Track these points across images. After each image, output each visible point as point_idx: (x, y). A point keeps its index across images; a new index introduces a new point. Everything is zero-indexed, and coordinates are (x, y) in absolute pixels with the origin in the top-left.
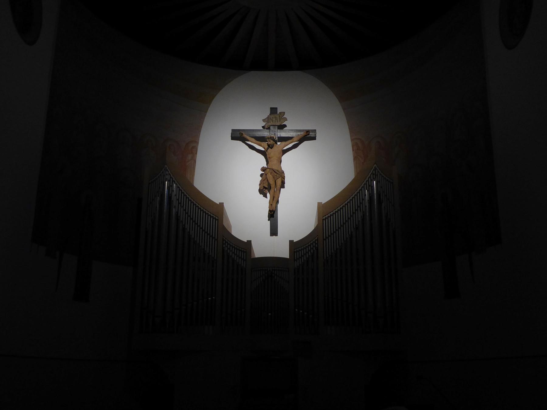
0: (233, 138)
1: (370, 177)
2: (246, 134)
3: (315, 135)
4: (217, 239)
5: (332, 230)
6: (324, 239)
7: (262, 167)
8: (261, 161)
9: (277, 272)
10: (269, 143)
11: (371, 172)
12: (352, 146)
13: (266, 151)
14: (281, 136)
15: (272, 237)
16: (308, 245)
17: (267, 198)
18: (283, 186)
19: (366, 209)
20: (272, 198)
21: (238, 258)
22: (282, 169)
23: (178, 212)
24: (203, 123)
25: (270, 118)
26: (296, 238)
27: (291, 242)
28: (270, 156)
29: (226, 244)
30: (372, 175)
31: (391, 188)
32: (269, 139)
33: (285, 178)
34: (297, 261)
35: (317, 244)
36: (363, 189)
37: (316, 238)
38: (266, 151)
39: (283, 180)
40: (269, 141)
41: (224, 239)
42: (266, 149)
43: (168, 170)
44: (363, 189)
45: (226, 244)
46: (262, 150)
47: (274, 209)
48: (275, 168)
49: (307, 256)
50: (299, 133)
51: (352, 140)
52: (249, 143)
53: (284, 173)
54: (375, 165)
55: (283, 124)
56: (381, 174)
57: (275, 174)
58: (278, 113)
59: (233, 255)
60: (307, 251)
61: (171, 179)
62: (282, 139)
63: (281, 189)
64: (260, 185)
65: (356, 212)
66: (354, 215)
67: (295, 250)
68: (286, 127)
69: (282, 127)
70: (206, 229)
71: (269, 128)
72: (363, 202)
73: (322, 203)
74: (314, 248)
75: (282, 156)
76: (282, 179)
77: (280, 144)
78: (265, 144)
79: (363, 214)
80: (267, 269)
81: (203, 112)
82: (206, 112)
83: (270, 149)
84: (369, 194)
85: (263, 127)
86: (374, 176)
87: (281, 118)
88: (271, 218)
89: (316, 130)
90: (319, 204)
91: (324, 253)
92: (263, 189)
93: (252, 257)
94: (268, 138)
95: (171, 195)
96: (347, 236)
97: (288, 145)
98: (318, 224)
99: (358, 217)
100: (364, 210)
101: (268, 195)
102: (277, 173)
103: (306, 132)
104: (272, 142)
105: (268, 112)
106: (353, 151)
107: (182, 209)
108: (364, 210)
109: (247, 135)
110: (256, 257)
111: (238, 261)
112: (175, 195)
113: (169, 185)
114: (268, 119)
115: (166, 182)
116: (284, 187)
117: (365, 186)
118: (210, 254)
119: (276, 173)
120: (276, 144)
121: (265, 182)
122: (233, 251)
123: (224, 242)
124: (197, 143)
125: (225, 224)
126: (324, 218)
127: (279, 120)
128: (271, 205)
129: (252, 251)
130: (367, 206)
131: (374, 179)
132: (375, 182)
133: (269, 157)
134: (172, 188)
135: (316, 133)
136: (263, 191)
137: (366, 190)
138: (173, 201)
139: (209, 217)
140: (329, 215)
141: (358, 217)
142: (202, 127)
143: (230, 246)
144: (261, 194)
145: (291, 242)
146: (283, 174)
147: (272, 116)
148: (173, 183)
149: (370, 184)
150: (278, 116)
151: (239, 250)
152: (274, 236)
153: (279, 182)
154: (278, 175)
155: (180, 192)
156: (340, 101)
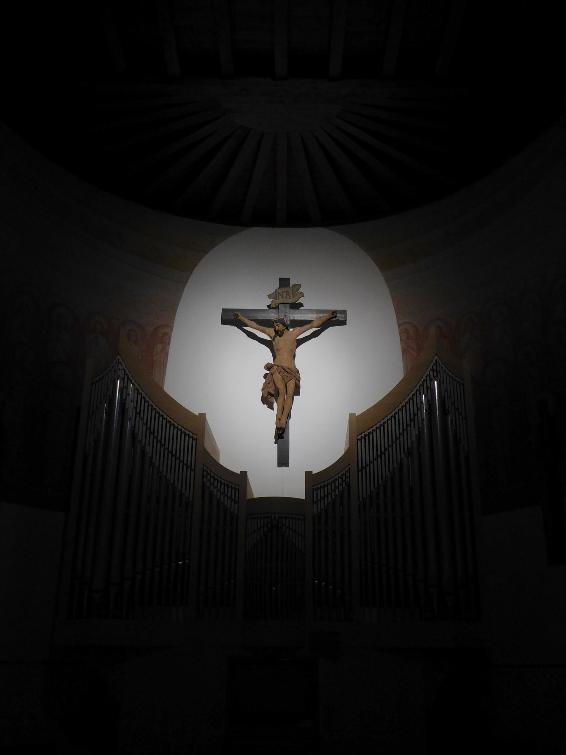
0: (225, 321)
1: (429, 375)
2: (242, 316)
3: (346, 317)
4: (194, 470)
5: (386, 442)
6: (358, 471)
7: (267, 364)
8: (266, 356)
9: (286, 521)
10: (277, 328)
11: (431, 367)
12: (399, 333)
13: (272, 341)
14: (295, 319)
15: (280, 468)
16: (338, 477)
17: (273, 410)
18: (297, 392)
19: (423, 424)
20: (281, 411)
21: (226, 498)
22: (296, 367)
23: (134, 427)
24: (180, 299)
25: (279, 292)
26: (316, 469)
27: (308, 474)
28: (279, 348)
29: (209, 477)
30: (431, 373)
31: (460, 393)
32: (276, 322)
33: (300, 380)
34: (317, 504)
35: (349, 477)
36: (418, 393)
37: (347, 468)
38: (272, 341)
39: (297, 382)
40: (277, 325)
41: (205, 468)
42: (273, 338)
43: (122, 363)
44: (418, 393)
45: (209, 477)
46: (267, 340)
47: (284, 426)
48: (285, 364)
49: (333, 496)
50: (321, 315)
51: (399, 325)
52: (245, 329)
53: (299, 372)
54: (436, 357)
55: (298, 303)
56: (445, 371)
57: (286, 374)
58: (291, 286)
59: (219, 493)
60: (333, 488)
61: (126, 377)
62: (296, 324)
63: (295, 396)
64: (263, 390)
65: (409, 428)
66: (405, 433)
67: (315, 487)
68: (303, 306)
69: (296, 306)
70: (178, 453)
71: (277, 308)
72: (418, 413)
73: (356, 414)
74: (344, 484)
75: (296, 349)
76: (296, 382)
77: (293, 330)
78: (271, 331)
79: (419, 432)
80: (271, 516)
81: (181, 285)
82: (185, 283)
83: (278, 336)
84: (428, 401)
85: (269, 307)
86: (435, 374)
87: (294, 293)
88: (279, 439)
89: (346, 310)
90: (351, 416)
91: (359, 489)
92: (268, 396)
93: (249, 497)
94: (276, 321)
95: (125, 400)
96: (395, 466)
97: (305, 332)
98: (349, 448)
99: (411, 435)
100: (420, 425)
101: (275, 405)
102: (288, 372)
103: (331, 313)
104: (280, 327)
105: (276, 285)
106: (401, 340)
107: (141, 422)
108: (420, 425)
109: (245, 317)
110: (255, 497)
111: (226, 504)
112: (131, 401)
113: (122, 386)
114: (276, 294)
115: (119, 382)
116: (298, 394)
117: (421, 388)
118: (183, 491)
119: (288, 372)
120: (288, 330)
121: (270, 385)
122: (219, 487)
123: (205, 474)
124: (172, 328)
125: (207, 446)
126: (359, 437)
127: (291, 296)
128: (280, 419)
129: (248, 489)
130: (425, 418)
131: (435, 378)
132: (436, 382)
133: (277, 349)
134: (127, 391)
135: (347, 314)
136: (267, 400)
137: (423, 396)
138: (127, 410)
139: (172, 427)
140: (367, 433)
141: (411, 435)
142: (178, 305)
143: (214, 480)
144: (264, 404)
145: (308, 474)
146: (297, 374)
147: (282, 290)
148: (129, 382)
149: (429, 385)
150: (290, 291)
151: (232, 488)
152: (284, 467)
153: (291, 385)
154: (290, 375)
155: (140, 396)
156: (381, 271)
